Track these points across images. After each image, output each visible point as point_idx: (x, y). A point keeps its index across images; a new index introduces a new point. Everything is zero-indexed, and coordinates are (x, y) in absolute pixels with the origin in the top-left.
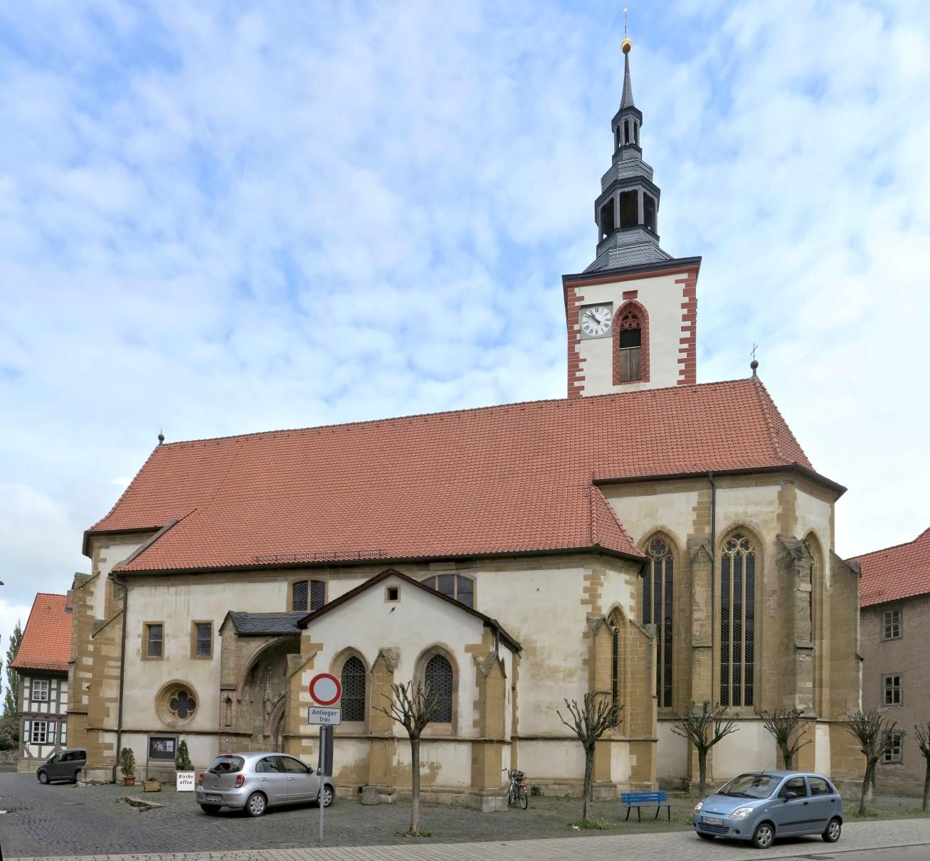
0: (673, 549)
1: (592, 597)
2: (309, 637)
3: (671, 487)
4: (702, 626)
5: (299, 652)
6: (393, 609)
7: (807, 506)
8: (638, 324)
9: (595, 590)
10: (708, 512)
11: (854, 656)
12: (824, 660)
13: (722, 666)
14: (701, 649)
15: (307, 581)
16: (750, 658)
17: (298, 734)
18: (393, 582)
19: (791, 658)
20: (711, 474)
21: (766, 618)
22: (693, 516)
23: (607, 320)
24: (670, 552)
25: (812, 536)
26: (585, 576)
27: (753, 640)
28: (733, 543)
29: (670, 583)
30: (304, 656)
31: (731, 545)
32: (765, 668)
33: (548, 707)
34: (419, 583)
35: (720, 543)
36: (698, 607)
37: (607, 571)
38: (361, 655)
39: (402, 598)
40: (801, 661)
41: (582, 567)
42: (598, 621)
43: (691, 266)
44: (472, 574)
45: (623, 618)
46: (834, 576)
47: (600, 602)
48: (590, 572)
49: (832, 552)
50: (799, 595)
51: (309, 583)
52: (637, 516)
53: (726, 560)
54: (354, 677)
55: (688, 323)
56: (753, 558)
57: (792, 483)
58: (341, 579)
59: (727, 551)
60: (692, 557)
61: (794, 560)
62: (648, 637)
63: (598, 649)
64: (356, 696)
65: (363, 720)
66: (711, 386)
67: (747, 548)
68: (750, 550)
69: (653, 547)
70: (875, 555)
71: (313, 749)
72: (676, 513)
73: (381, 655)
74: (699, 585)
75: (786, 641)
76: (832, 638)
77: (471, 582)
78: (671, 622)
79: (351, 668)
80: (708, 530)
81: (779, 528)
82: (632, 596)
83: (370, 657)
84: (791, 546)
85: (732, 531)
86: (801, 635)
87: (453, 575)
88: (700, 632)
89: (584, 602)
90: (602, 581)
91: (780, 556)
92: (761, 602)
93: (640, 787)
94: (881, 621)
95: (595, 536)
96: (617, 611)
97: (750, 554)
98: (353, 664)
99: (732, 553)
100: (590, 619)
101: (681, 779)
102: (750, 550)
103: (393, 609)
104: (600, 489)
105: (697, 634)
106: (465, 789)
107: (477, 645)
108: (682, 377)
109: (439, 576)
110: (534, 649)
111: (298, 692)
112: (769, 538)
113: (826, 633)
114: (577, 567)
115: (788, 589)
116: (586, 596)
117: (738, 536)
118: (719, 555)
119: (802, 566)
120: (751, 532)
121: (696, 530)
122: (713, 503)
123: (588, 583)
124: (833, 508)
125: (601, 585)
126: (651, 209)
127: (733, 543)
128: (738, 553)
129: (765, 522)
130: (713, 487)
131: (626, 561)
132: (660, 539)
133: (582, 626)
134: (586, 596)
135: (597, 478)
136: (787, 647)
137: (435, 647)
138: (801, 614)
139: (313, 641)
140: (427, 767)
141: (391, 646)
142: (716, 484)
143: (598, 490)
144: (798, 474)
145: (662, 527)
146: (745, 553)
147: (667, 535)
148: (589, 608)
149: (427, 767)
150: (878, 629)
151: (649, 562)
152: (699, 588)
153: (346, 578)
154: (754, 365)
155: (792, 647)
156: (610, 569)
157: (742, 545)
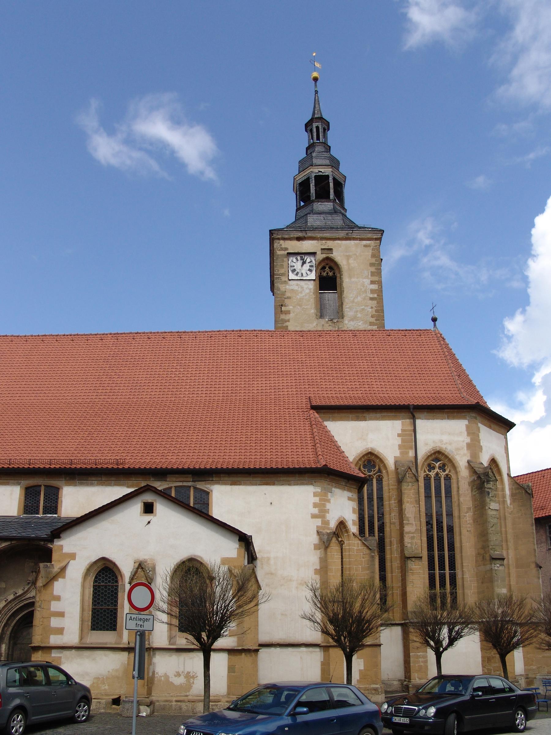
0: (382, 468)
1: (321, 512)
2: (62, 546)
3: (378, 415)
4: (413, 538)
5: (50, 561)
6: (149, 522)
7: (488, 438)
8: (334, 273)
9: (324, 505)
10: (411, 438)
11: (533, 566)
12: (511, 568)
13: (429, 574)
14: (413, 559)
15: (41, 486)
16: (452, 566)
17: (48, 645)
18: (148, 497)
19: (488, 567)
20: (412, 407)
21: (464, 531)
22: (398, 441)
23: (297, 260)
24: (380, 471)
25: (493, 461)
26: (314, 493)
27: (454, 550)
28: (432, 465)
29: (381, 499)
30: (56, 566)
31: (431, 468)
32: (467, 576)
33: (282, 614)
34: (161, 491)
35: (423, 464)
36: (409, 521)
37: (333, 489)
38: (115, 564)
39: (158, 511)
40: (496, 570)
41: (312, 484)
42: (328, 534)
43: (377, 235)
44: (209, 486)
45: (347, 531)
46: (512, 495)
47: (329, 517)
48: (318, 490)
49: (509, 475)
50: (490, 513)
51: (43, 489)
52: (353, 438)
53: (427, 479)
54: (106, 587)
55: (376, 278)
56: (450, 478)
57: (476, 418)
58: (76, 486)
59: (428, 473)
60: (400, 477)
61: (484, 482)
62: (371, 549)
63: (330, 560)
64: (108, 605)
65: (115, 630)
66: (401, 332)
67: (444, 471)
68: (447, 472)
69: (365, 466)
70: (534, 474)
71: (62, 660)
72: (382, 437)
73: (141, 566)
74: (408, 502)
75: (482, 552)
76: (516, 549)
77: (207, 494)
78: (384, 533)
79: (103, 577)
80: (411, 454)
81: (469, 455)
82: (354, 512)
83: (126, 569)
84: (480, 471)
85: (431, 455)
86: (494, 547)
87: (190, 487)
88: (411, 543)
89: (314, 516)
90: (329, 498)
91: (472, 479)
92: (459, 517)
93: (368, 690)
94: (546, 532)
95: (321, 457)
96: (342, 525)
97: (447, 475)
98: (105, 574)
99: (432, 474)
100: (321, 532)
101: (399, 680)
102: (447, 472)
103: (149, 522)
104: (317, 412)
105: (409, 545)
106: (221, 697)
107: (232, 558)
108: (373, 320)
109: (176, 487)
110: (269, 559)
111: (50, 602)
112: (462, 461)
113: (511, 545)
114: (307, 484)
115: (480, 507)
116: (316, 511)
117: (437, 460)
118: (422, 475)
119: (490, 488)
120: (446, 457)
121: (401, 453)
122: (415, 431)
123: (317, 500)
124: (506, 438)
125: (329, 501)
126: (339, 189)
127: (432, 465)
128: (437, 474)
129: (458, 449)
130: (414, 418)
131: (348, 480)
132: (371, 459)
133: (314, 539)
134: (316, 511)
135: (314, 404)
136: (483, 557)
137: (191, 560)
138: (493, 529)
139: (66, 550)
140: (182, 677)
141: (146, 557)
142: (416, 415)
143: (316, 414)
144: (480, 412)
145: (372, 449)
146: (443, 474)
147: (377, 457)
148: (319, 522)
149: (182, 677)
150: (544, 537)
151: (361, 477)
152: (408, 504)
153: (81, 484)
154: (434, 320)
155: (488, 558)
156: (335, 487)
157: (440, 468)
